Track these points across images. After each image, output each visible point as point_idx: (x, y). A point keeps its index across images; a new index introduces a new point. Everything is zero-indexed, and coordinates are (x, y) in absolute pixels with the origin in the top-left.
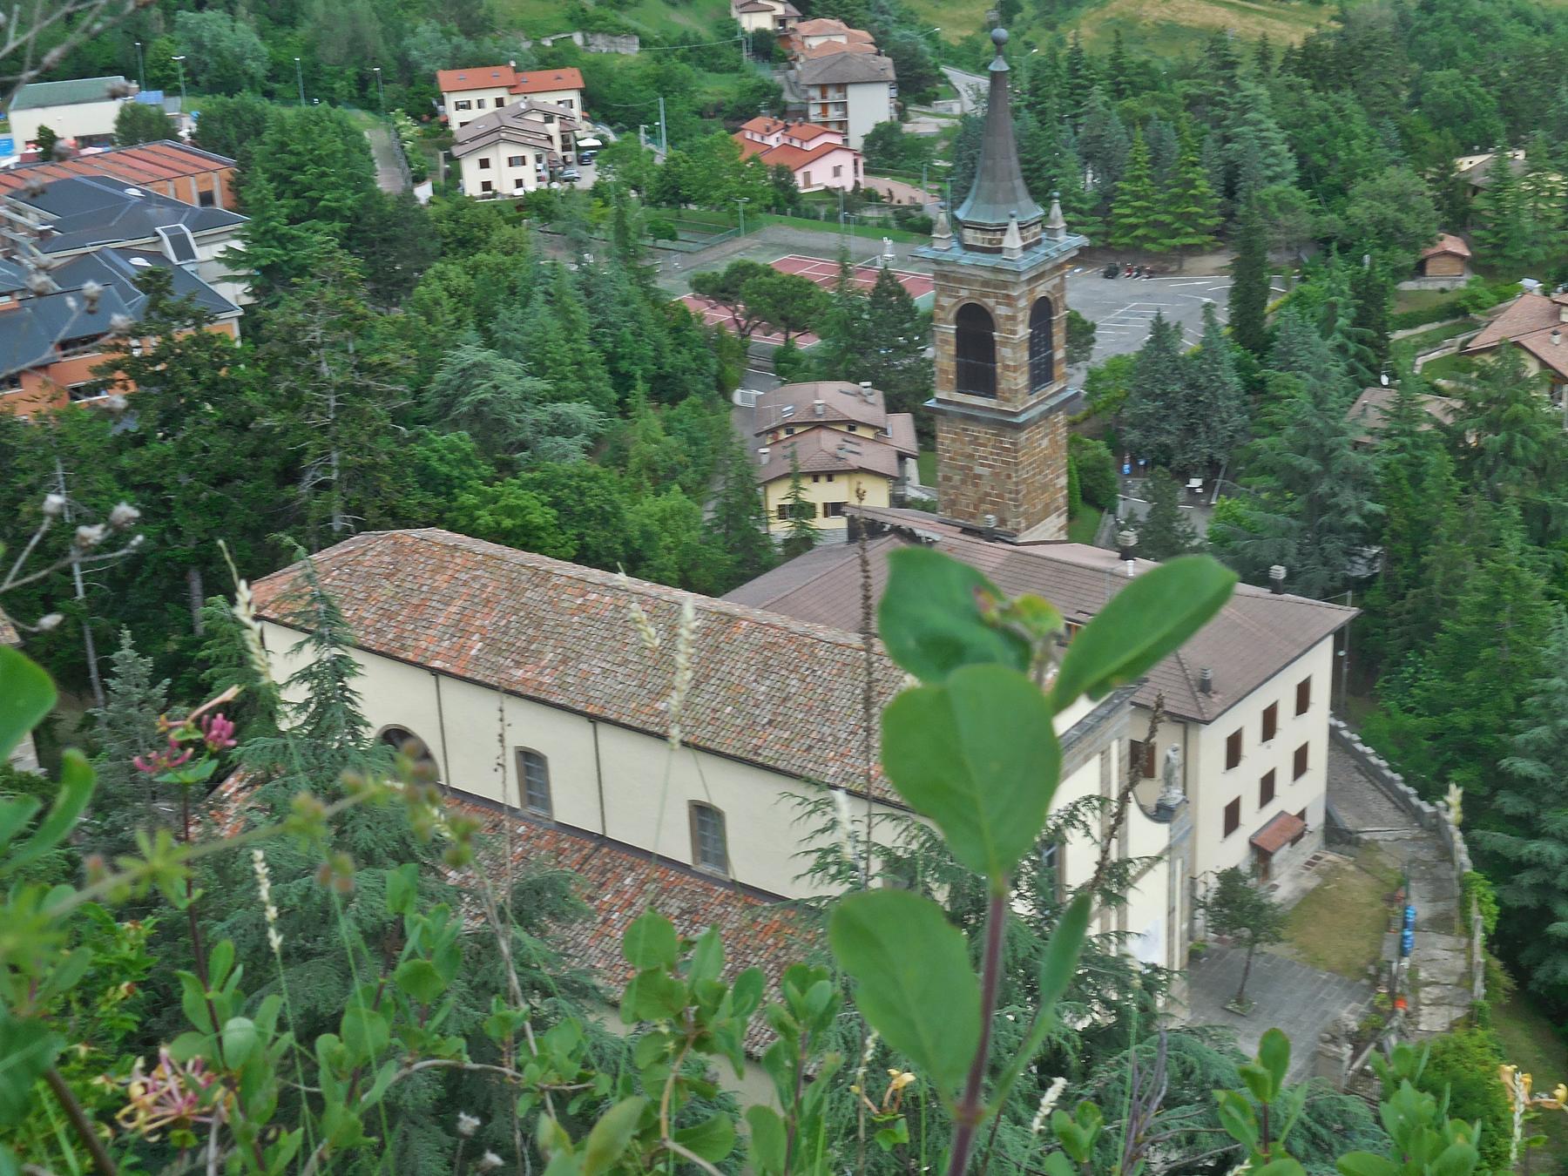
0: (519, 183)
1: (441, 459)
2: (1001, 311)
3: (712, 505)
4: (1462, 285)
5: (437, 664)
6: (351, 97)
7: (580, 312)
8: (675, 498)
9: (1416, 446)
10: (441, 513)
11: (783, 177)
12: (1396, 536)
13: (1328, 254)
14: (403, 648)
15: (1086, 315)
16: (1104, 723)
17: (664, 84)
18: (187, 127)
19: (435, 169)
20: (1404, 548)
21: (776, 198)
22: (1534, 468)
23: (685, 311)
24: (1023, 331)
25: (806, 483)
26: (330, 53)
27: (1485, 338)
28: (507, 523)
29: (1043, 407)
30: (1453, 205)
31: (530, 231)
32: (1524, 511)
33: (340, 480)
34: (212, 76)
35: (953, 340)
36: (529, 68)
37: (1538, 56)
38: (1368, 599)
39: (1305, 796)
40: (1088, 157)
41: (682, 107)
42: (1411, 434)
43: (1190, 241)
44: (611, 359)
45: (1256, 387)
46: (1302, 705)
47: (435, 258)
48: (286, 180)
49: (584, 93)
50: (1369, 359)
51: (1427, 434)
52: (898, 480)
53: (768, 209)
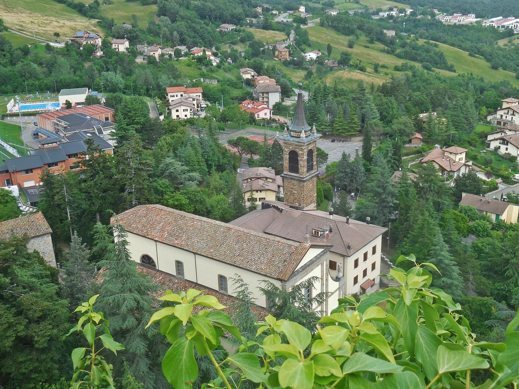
0: (186, 116)
1: (161, 186)
2: (300, 152)
3: (231, 198)
4: (420, 146)
5: (156, 239)
6: (145, 94)
7: (199, 149)
8: (221, 196)
9: (407, 186)
10: (160, 200)
11: (252, 116)
12: (402, 209)
13: (387, 137)
14: (148, 235)
15: (326, 152)
16: (322, 257)
17: (223, 91)
18: (103, 100)
19: (165, 112)
20: (404, 212)
21: (250, 121)
22: (436, 192)
23: (226, 149)
24: (305, 157)
25: (254, 193)
26: (140, 82)
27: (426, 159)
28: (176, 203)
29: (310, 176)
30: (418, 126)
31: (188, 128)
32: (434, 203)
33: (135, 191)
34: (111, 88)
36: (189, 87)
37: (440, 89)
38: (395, 224)
39: (375, 275)
40: (328, 112)
41: (227, 97)
42: (406, 183)
43: (353, 133)
44: (207, 161)
45: (368, 170)
46: (374, 252)
47: (163, 134)
48: (127, 115)
49: (202, 93)
50: (396, 163)
51: (410, 183)
52: (278, 192)
53: (248, 123)
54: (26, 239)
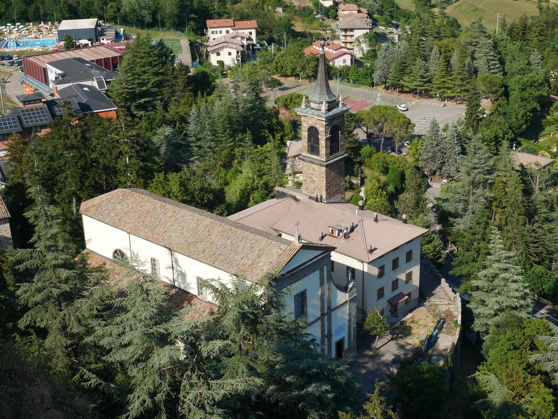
35: (307, 137)
54: (333, 249)
